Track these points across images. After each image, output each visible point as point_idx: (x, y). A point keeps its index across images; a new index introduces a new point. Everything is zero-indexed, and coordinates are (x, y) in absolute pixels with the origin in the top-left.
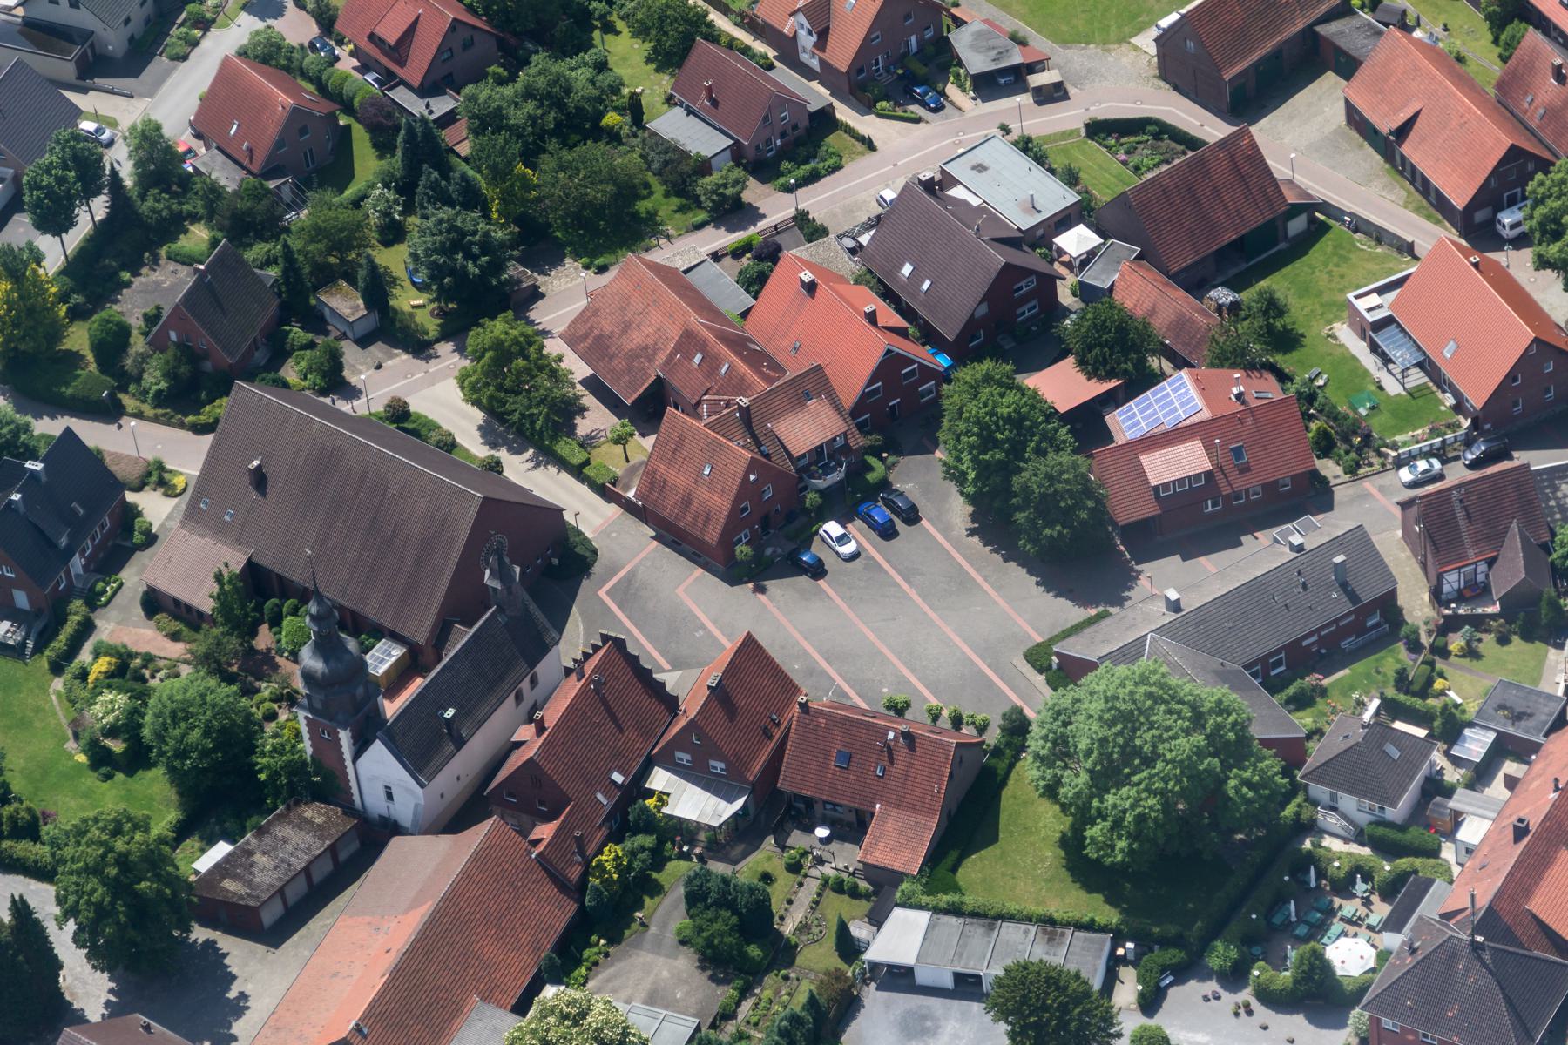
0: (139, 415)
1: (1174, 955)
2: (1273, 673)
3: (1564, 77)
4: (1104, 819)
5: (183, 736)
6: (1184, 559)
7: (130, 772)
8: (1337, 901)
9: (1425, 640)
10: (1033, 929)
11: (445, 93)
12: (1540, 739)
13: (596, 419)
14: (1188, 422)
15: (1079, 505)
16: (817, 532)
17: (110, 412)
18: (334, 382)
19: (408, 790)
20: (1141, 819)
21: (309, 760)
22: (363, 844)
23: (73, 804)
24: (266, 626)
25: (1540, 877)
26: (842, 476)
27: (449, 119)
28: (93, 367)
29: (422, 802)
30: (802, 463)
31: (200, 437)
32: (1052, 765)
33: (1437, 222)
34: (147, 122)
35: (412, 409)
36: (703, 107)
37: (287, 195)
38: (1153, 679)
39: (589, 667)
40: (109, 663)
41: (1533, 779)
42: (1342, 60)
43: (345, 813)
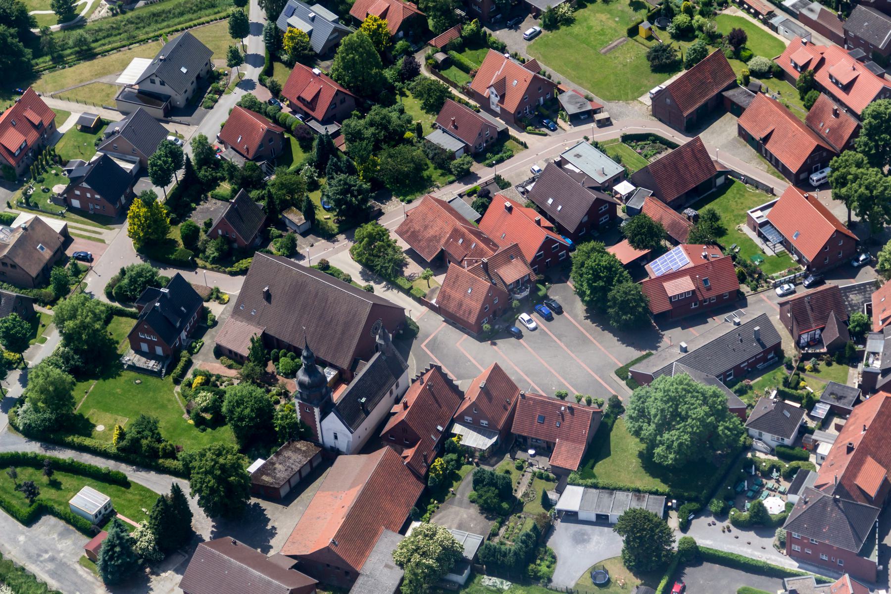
0: (205, 268)
1: (695, 506)
2: (728, 379)
3: (838, 114)
4: (663, 445)
5: (242, 411)
6: (683, 329)
7: (214, 428)
8: (764, 481)
9: (794, 364)
10: (630, 494)
11: (333, 123)
12: (850, 408)
13: (413, 268)
14: (683, 268)
15: (638, 305)
16: (517, 318)
17: (192, 266)
18: (292, 252)
19: (345, 435)
20: (681, 444)
21: (298, 421)
22: (323, 458)
24: (271, 361)
25: (860, 469)
26: (528, 293)
27: (337, 134)
28: (182, 246)
30: (510, 287)
32: (637, 421)
33: (782, 179)
34: (201, 136)
35: (330, 264)
36: (450, 129)
37: (264, 169)
38: (685, 382)
39: (426, 378)
41: (850, 426)
42: (735, 107)
43: (315, 445)
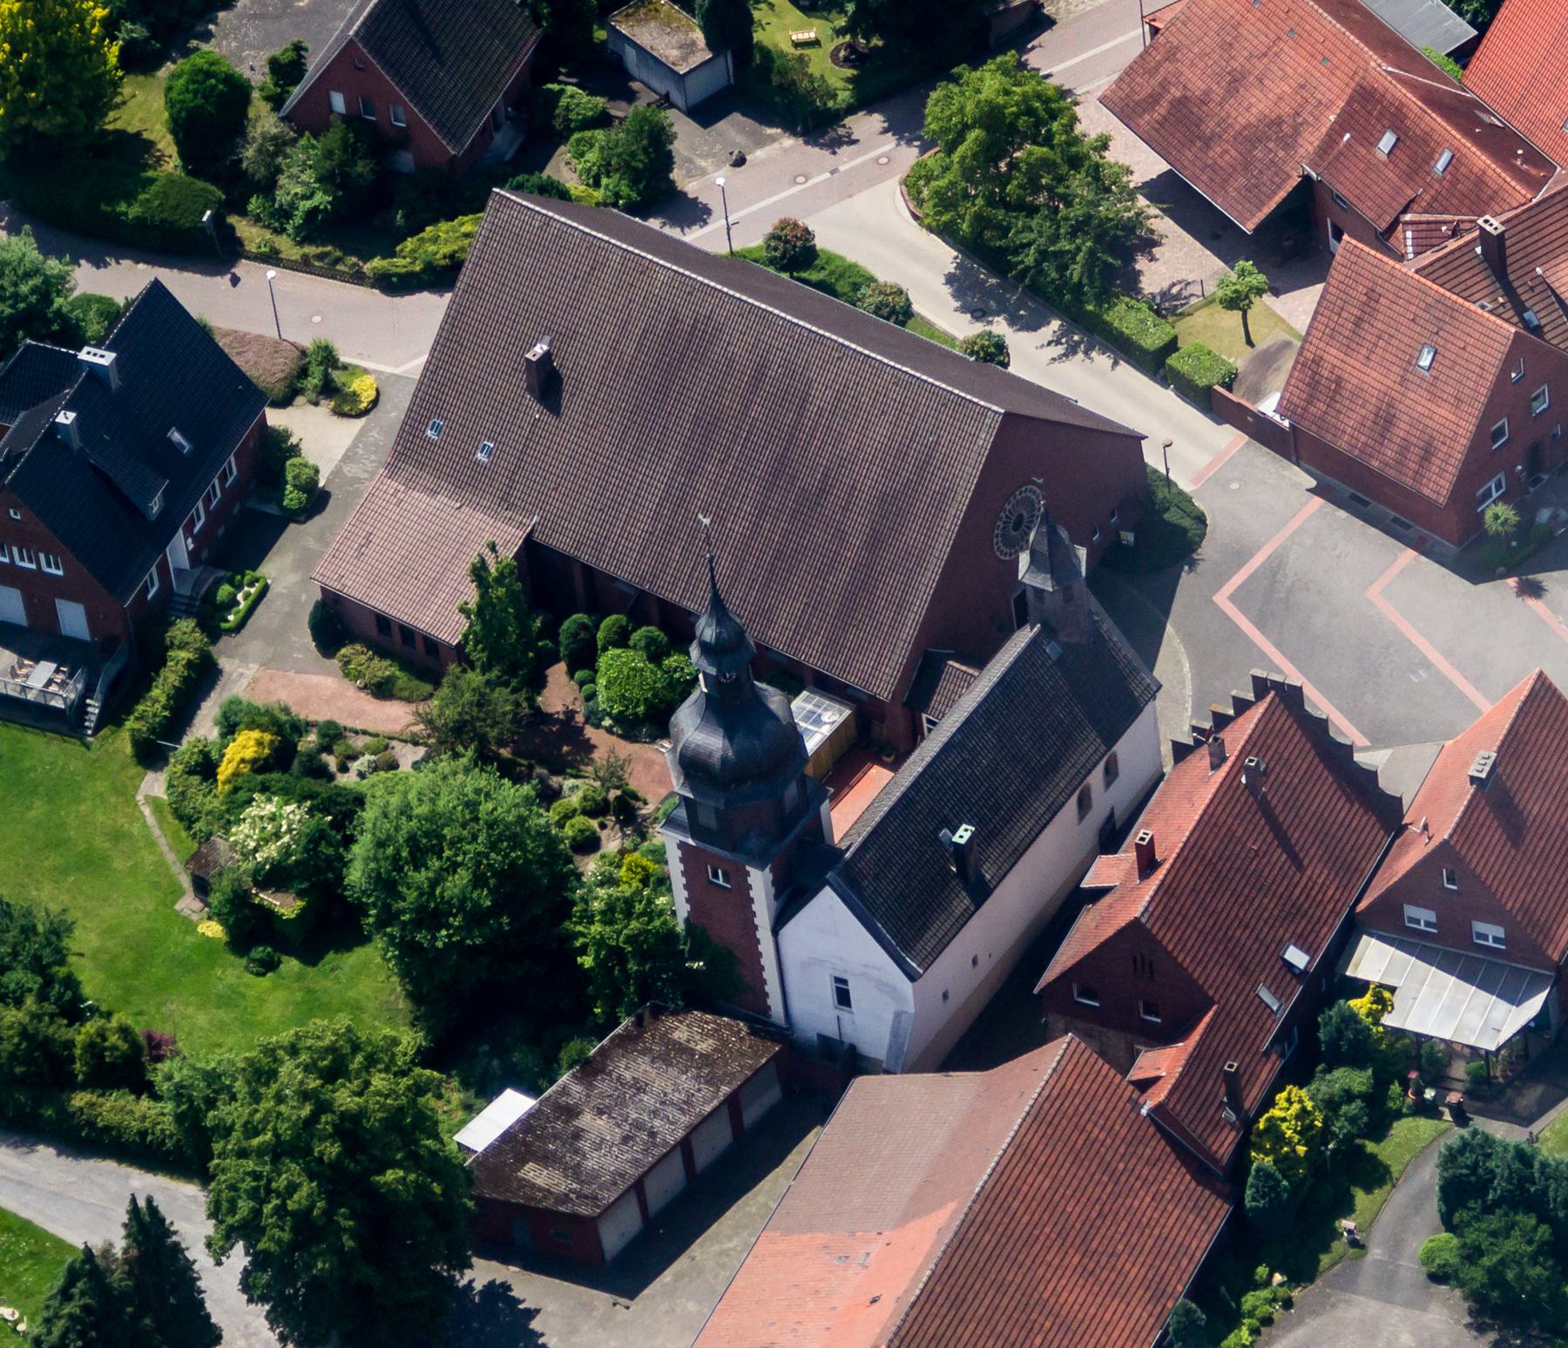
0: (271, 258)
5: (434, 883)
7: (311, 955)
21: (680, 928)
22: (787, 1092)
23: (202, 1019)
24: (562, 667)
29: (911, 1009)
31: (397, 300)
35: (820, 243)
39: (1236, 737)
40: (260, 743)
43: (753, 1032)
